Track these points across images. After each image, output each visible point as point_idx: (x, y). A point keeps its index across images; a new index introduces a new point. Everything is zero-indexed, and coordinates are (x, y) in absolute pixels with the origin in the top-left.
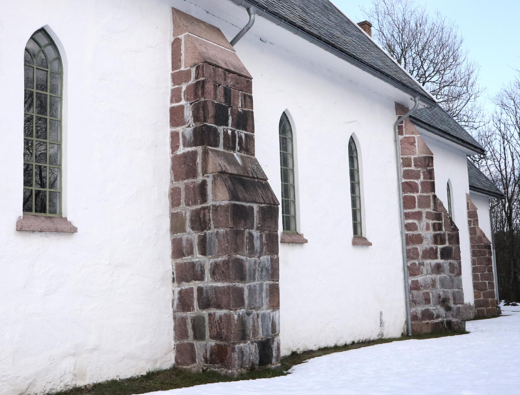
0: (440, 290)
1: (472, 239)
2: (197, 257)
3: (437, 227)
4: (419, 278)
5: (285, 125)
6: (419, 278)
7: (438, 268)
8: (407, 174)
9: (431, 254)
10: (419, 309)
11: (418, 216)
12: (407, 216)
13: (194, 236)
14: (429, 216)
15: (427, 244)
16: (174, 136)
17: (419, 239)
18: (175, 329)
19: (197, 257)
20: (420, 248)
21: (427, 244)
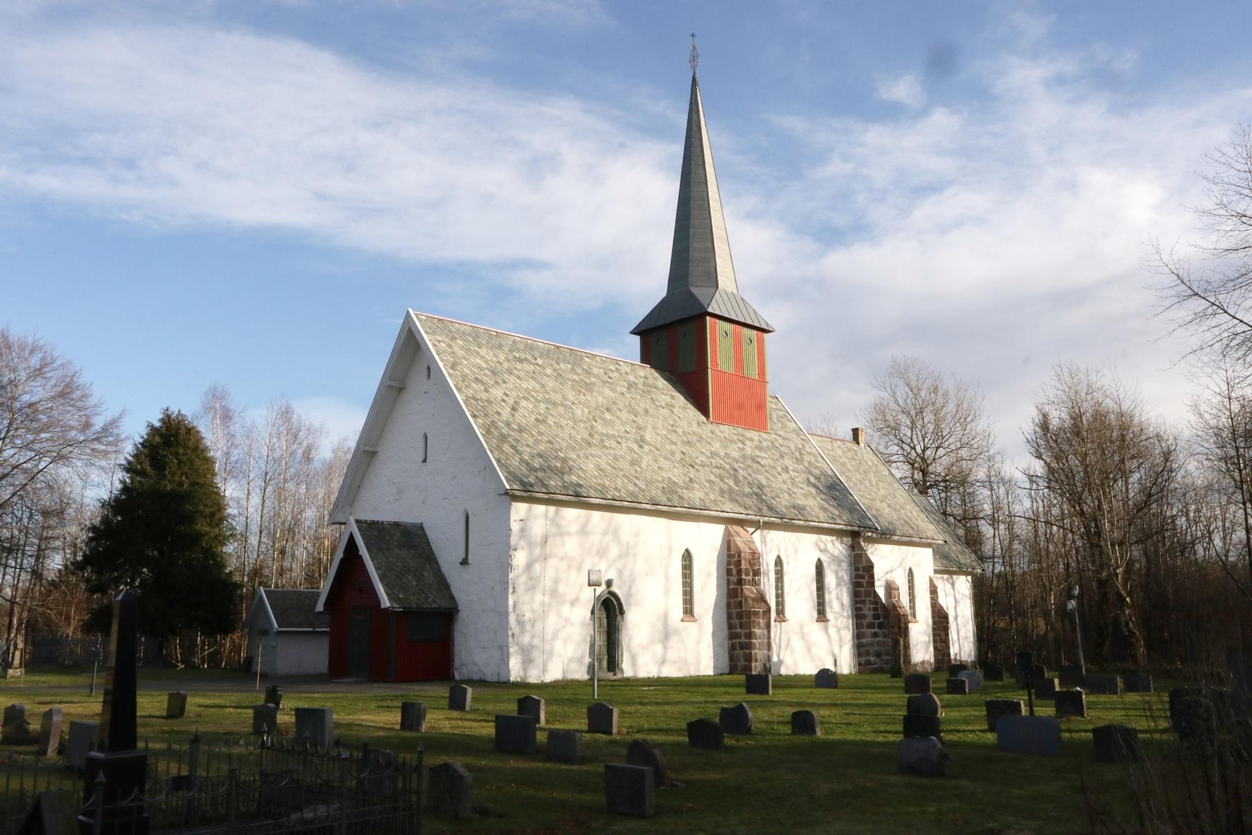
0: (876, 648)
1: (858, 616)
2: (739, 630)
3: (875, 609)
4: (864, 641)
5: (779, 562)
6: (864, 641)
7: (875, 635)
8: (857, 576)
9: (871, 626)
10: (863, 659)
11: (863, 602)
12: (856, 602)
13: (737, 622)
14: (871, 602)
15: (870, 619)
16: (728, 580)
17: (864, 617)
18: (797, 676)
19: (739, 630)
20: (864, 622)
21: (870, 619)
